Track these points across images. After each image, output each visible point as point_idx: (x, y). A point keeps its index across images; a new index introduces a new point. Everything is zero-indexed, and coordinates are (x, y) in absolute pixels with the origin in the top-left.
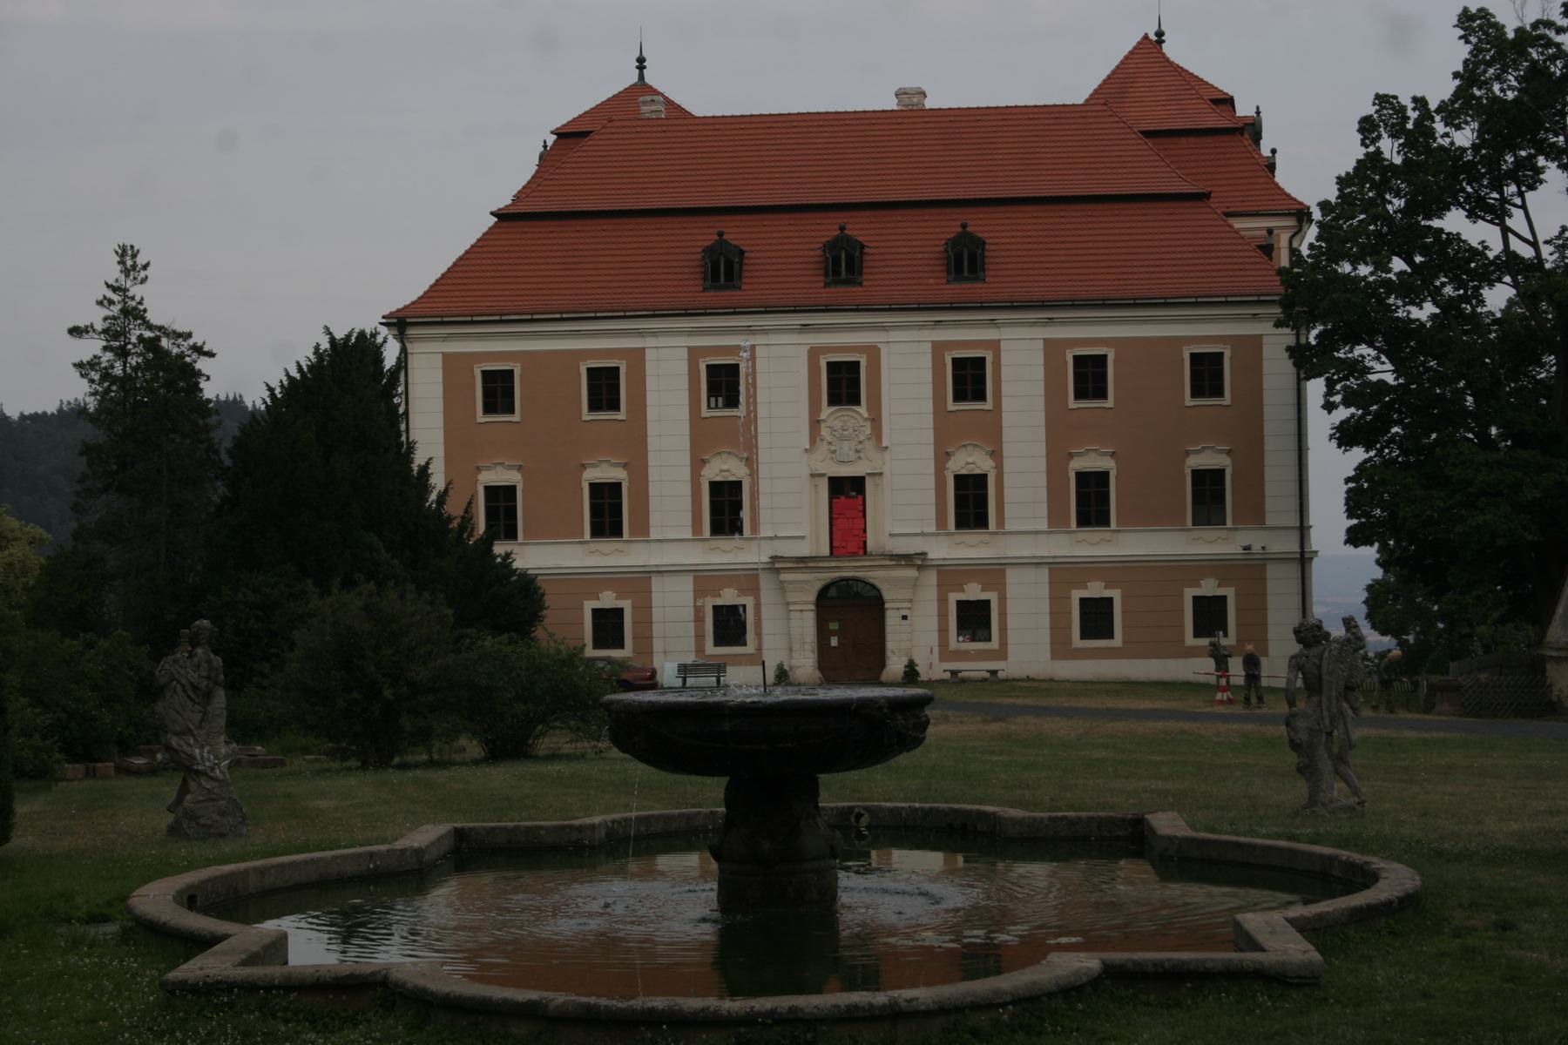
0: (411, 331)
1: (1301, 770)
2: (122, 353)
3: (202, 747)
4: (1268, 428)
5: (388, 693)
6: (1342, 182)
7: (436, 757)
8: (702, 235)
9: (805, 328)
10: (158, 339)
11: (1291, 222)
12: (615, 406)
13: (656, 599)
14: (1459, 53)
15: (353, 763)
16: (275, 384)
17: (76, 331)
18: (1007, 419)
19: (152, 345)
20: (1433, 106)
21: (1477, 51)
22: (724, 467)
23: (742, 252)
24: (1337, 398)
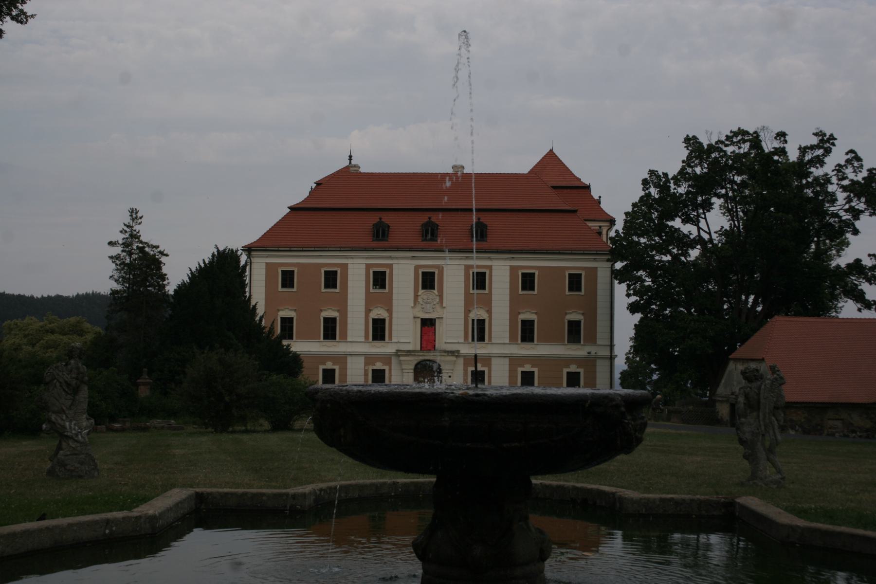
0: (253, 253)
1: (746, 457)
2: (130, 254)
3: (71, 421)
4: (599, 304)
5: (227, 399)
6: (634, 205)
7: (249, 428)
8: (374, 219)
9: (413, 258)
10: (144, 247)
11: (607, 224)
12: (335, 286)
13: (349, 366)
14: (684, 153)
15: (210, 429)
16: (194, 270)
17: (111, 244)
18: (494, 297)
19: (141, 250)
20: (670, 177)
21: (691, 152)
22: (379, 313)
23: (389, 227)
24: (631, 292)
